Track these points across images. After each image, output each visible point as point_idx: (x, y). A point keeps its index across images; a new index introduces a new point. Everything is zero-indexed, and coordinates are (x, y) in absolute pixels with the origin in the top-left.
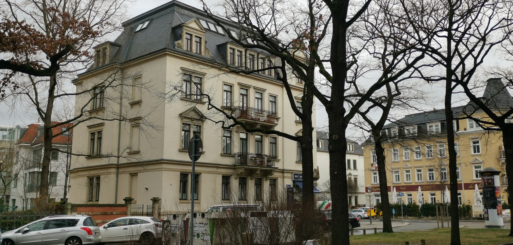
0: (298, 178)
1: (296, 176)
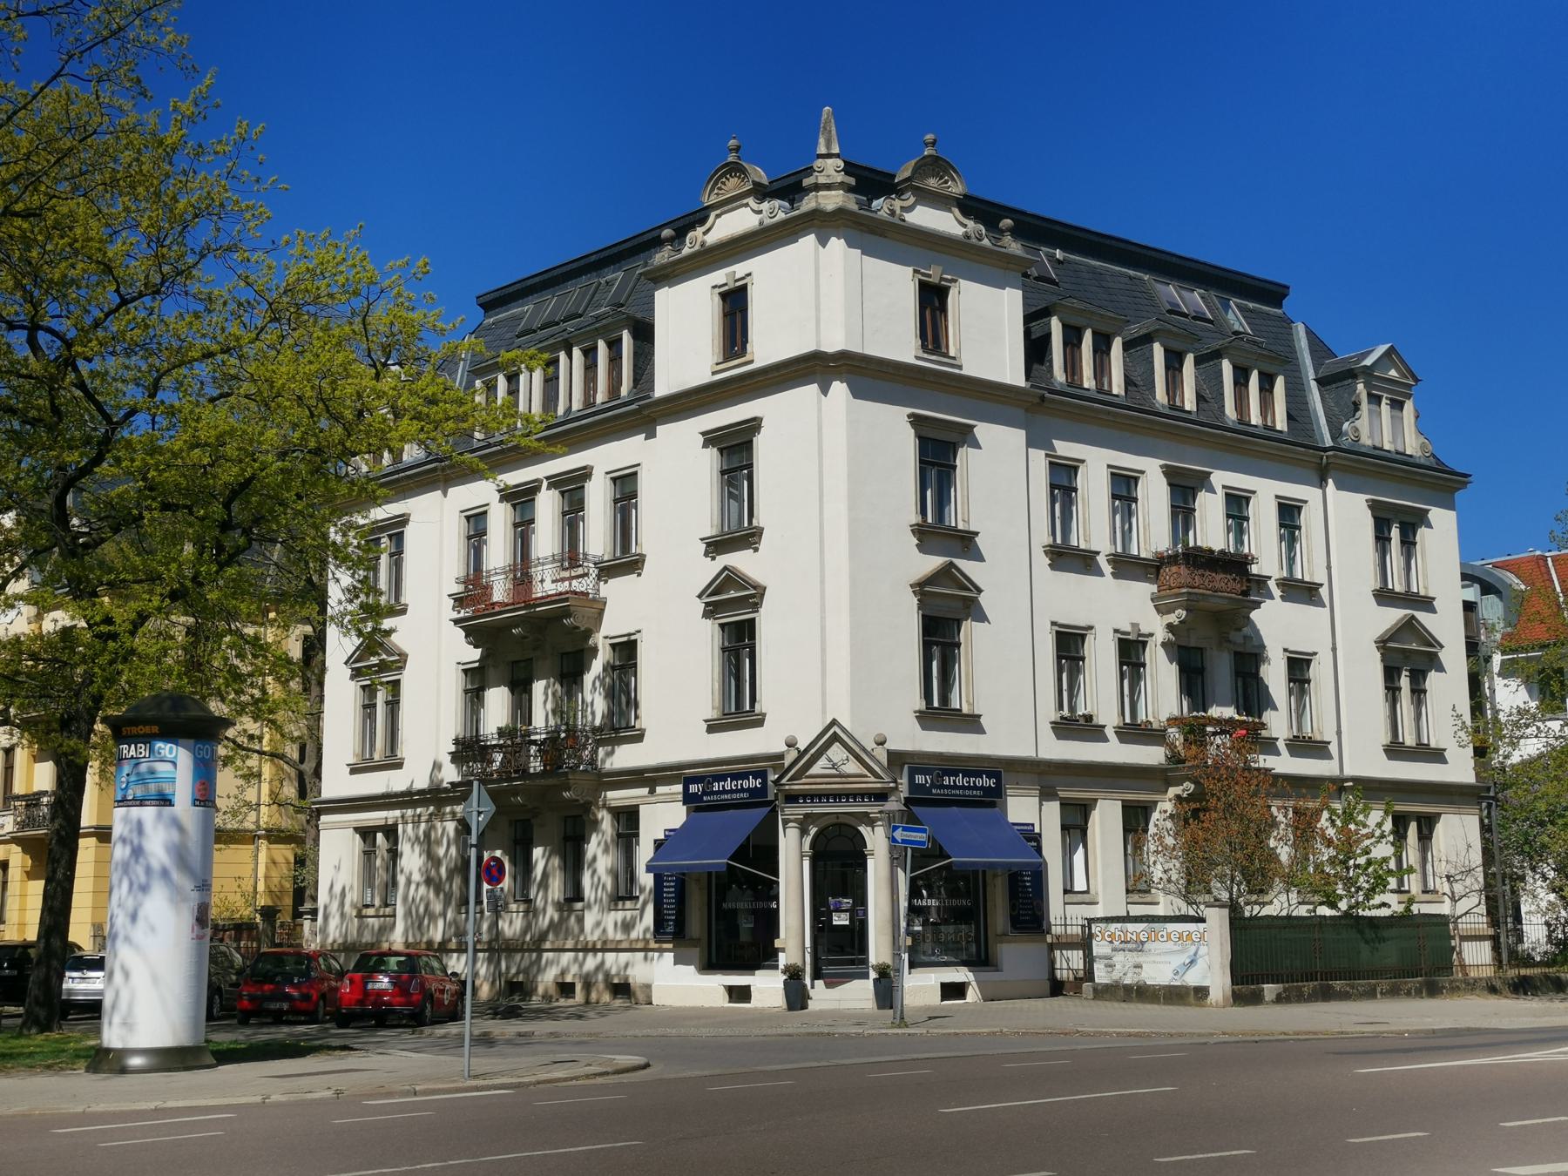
0: (704, 793)
1: (693, 788)
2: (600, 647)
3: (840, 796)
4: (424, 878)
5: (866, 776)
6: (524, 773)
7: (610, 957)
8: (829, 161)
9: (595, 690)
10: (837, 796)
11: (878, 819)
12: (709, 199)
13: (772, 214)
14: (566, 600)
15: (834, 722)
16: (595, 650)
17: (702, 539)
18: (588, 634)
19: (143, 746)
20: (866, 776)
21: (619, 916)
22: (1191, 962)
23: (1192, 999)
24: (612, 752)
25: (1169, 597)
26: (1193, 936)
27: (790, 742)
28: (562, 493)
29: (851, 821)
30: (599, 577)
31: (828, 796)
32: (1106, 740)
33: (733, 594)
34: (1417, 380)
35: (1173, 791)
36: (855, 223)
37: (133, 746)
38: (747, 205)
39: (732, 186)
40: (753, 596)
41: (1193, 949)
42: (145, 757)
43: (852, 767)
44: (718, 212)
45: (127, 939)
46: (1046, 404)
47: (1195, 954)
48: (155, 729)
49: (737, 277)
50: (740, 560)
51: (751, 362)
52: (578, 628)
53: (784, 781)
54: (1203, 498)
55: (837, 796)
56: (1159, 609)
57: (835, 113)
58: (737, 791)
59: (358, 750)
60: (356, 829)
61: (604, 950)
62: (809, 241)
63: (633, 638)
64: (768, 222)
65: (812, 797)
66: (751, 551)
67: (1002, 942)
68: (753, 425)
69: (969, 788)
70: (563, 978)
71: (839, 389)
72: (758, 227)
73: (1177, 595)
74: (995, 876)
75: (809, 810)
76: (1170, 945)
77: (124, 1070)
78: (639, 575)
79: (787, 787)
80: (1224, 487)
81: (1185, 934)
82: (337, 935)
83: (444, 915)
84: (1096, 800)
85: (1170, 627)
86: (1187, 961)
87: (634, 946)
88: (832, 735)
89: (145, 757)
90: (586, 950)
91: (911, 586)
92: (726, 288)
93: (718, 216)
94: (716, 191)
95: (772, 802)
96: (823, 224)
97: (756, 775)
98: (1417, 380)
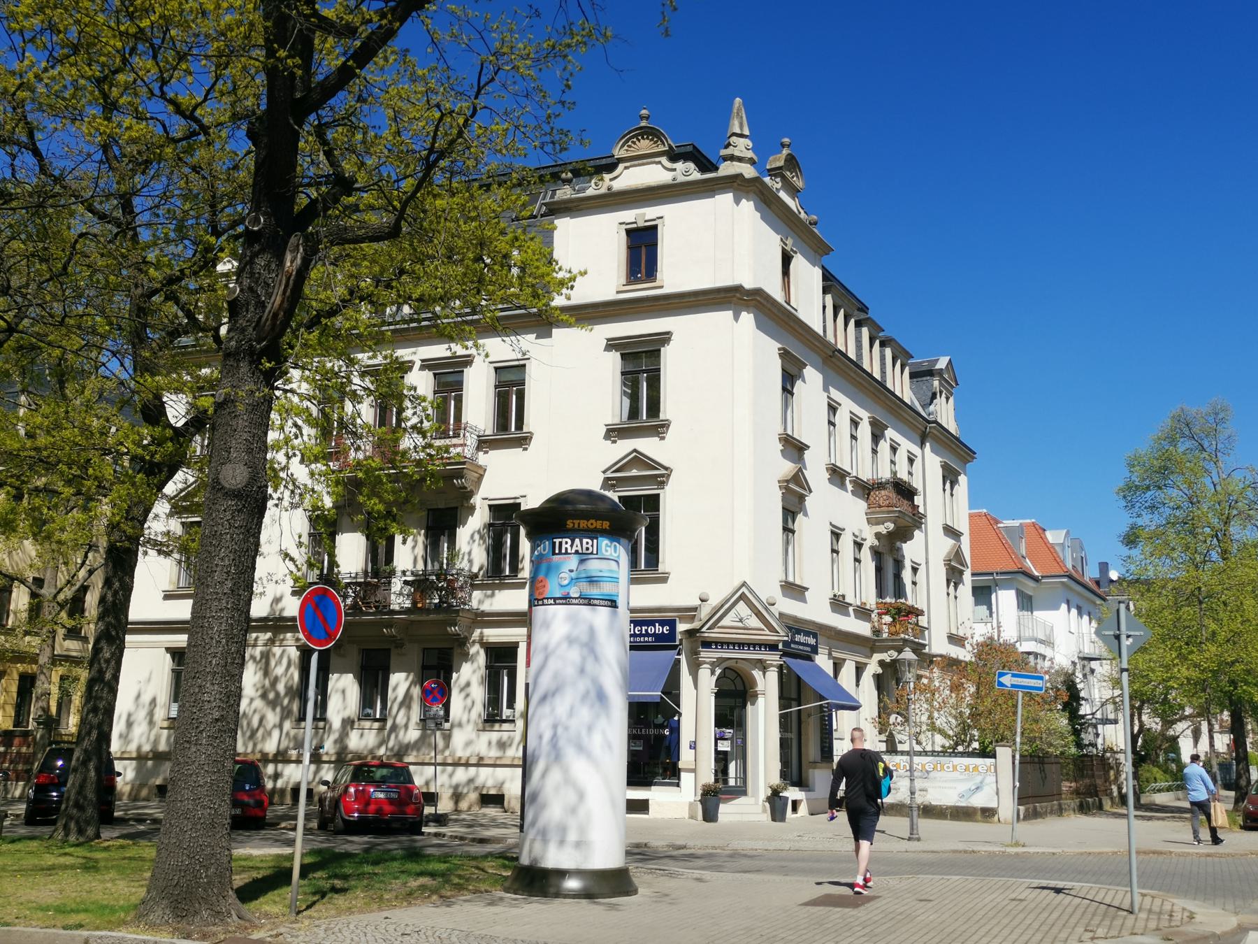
2: (478, 507)
3: (743, 644)
4: (259, 693)
5: (763, 630)
6: (383, 608)
7: (484, 772)
8: (742, 140)
9: (474, 541)
10: (741, 645)
11: (772, 665)
12: (619, 152)
13: (687, 173)
14: (464, 463)
15: (744, 584)
16: (472, 509)
17: (851, 412)
18: (471, 494)
19: (589, 541)
20: (763, 630)
21: (494, 736)
22: (977, 788)
23: (979, 816)
24: (493, 595)
25: (883, 512)
26: (980, 769)
27: (704, 597)
28: (435, 375)
29: (741, 665)
30: (479, 448)
31: (728, 644)
32: (847, 615)
33: (634, 472)
34: (957, 384)
35: (877, 657)
36: (760, 191)
37: (577, 541)
38: (660, 163)
39: (645, 146)
40: (662, 476)
41: (979, 779)
42: (592, 553)
43: (754, 622)
44: (628, 164)
45: (581, 748)
46: (833, 359)
47: (981, 783)
48: (606, 525)
49: (647, 218)
50: (648, 446)
51: (662, 287)
52: (466, 488)
53: (704, 630)
54: (882, 442)
55: (741, 645)
56: (869, 521)
57: (744, 104)
58: (641, 635)
59: (175, 579)
60: (168, 649)
61: (478, 765)
62: (728, 197)
63: (518, 501)
64: (681, 179)
65: (722, 644)
66: (657, 439)
67: (815, 768)
68: (664, 338)
69: (641, 635)
70: (428, 788)
71: (747, 318)
72: (671, 182)
73: (889, 512)
74: (809, 716)
75: (719, 655)
76: (956, 775)
77: (559, 894)
78: (525, 449)
79: (706, 635)
80: (891, 439)
81: (971, 767)
82: (144, 739)
83: (281, 726)
84: (845, 660)
85: (878, 536)
86: (973, 788)
87: (498, 763)
88: (743, 595)
89: (592, 553)
90: (456, 764)
91: (779, 482)
92: (635, 226)
93: (626, 168)
94: (626, 148)
95: (677, 646)
96: (737, 185)
97: (663, 623)
98: (957, 384)
